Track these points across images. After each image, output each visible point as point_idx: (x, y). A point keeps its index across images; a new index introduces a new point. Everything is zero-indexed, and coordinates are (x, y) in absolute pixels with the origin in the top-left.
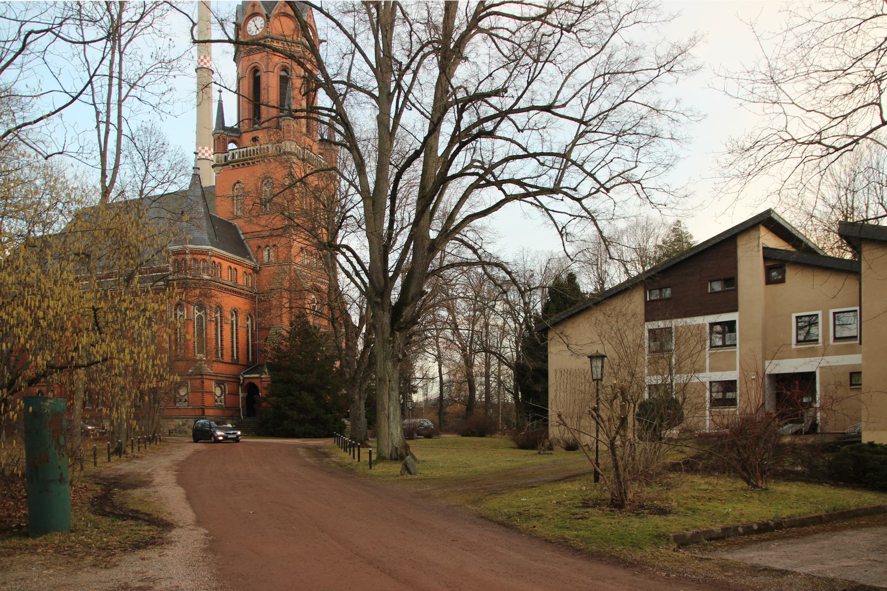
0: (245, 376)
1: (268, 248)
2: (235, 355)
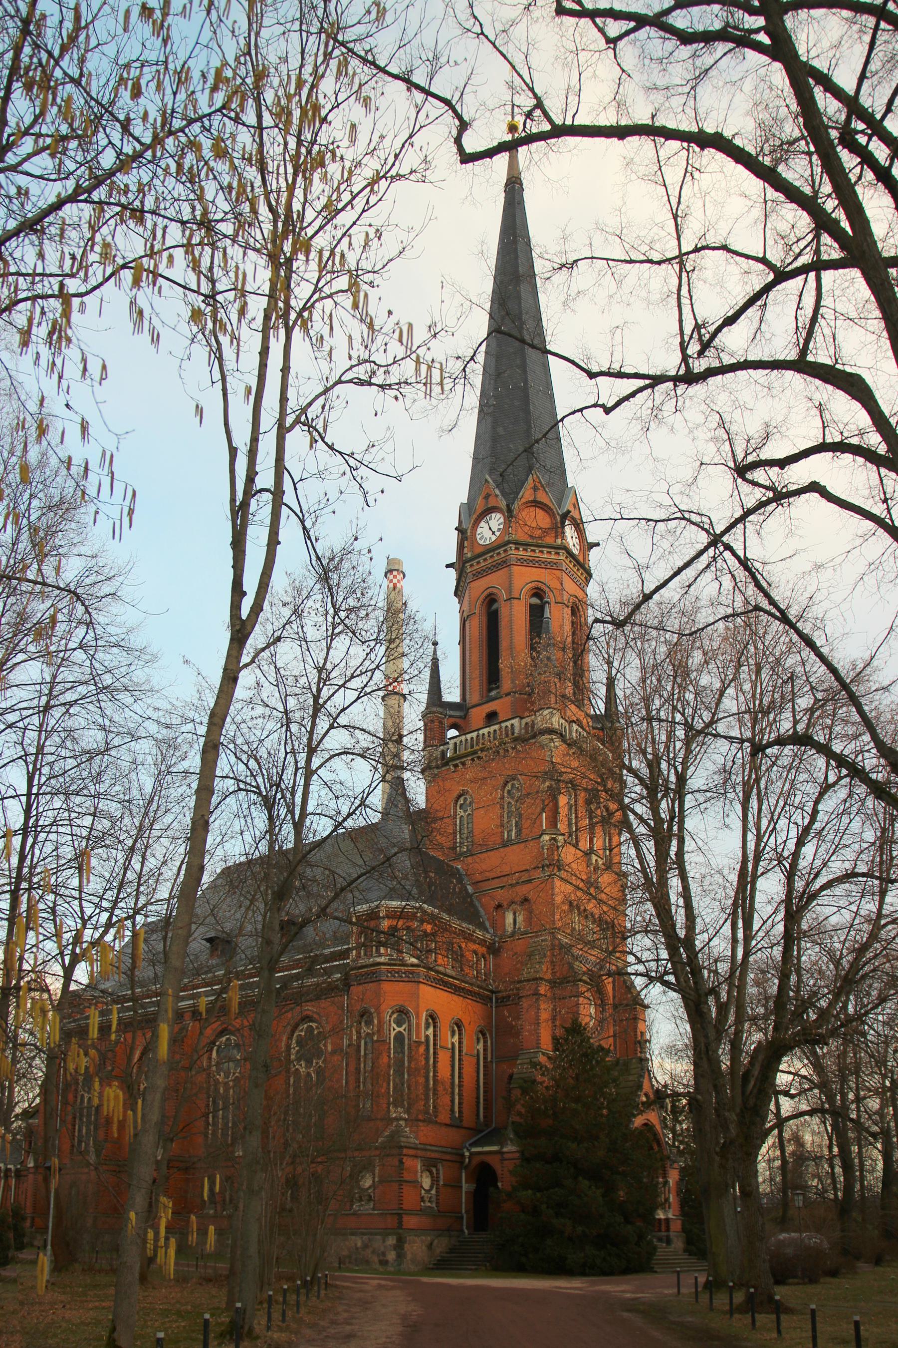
0: (474, 1150)
1: (514, 906)
2: (456, 1109)
